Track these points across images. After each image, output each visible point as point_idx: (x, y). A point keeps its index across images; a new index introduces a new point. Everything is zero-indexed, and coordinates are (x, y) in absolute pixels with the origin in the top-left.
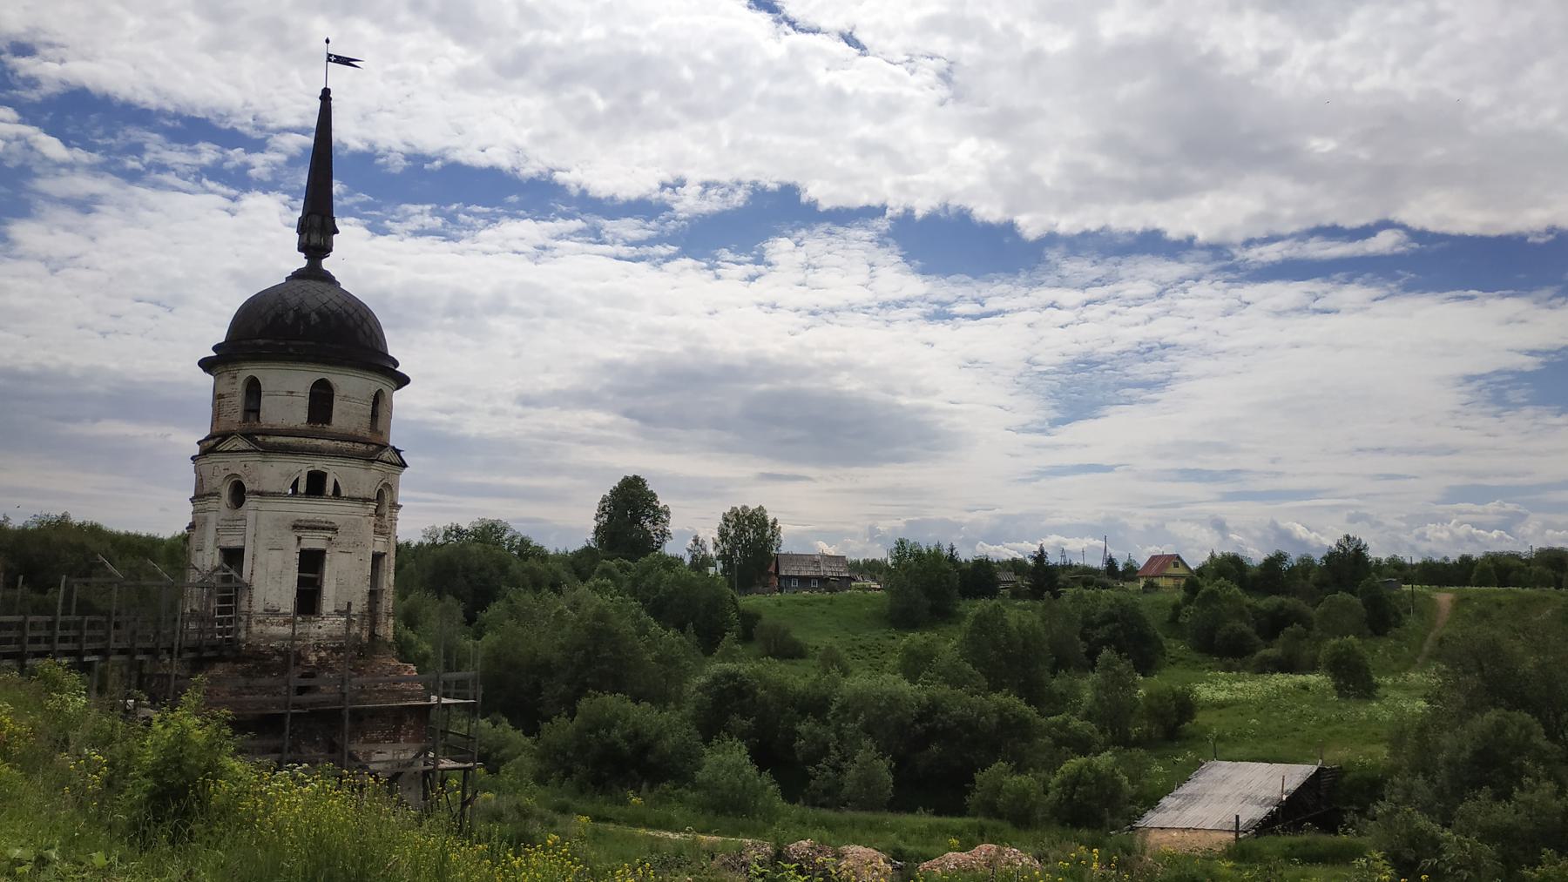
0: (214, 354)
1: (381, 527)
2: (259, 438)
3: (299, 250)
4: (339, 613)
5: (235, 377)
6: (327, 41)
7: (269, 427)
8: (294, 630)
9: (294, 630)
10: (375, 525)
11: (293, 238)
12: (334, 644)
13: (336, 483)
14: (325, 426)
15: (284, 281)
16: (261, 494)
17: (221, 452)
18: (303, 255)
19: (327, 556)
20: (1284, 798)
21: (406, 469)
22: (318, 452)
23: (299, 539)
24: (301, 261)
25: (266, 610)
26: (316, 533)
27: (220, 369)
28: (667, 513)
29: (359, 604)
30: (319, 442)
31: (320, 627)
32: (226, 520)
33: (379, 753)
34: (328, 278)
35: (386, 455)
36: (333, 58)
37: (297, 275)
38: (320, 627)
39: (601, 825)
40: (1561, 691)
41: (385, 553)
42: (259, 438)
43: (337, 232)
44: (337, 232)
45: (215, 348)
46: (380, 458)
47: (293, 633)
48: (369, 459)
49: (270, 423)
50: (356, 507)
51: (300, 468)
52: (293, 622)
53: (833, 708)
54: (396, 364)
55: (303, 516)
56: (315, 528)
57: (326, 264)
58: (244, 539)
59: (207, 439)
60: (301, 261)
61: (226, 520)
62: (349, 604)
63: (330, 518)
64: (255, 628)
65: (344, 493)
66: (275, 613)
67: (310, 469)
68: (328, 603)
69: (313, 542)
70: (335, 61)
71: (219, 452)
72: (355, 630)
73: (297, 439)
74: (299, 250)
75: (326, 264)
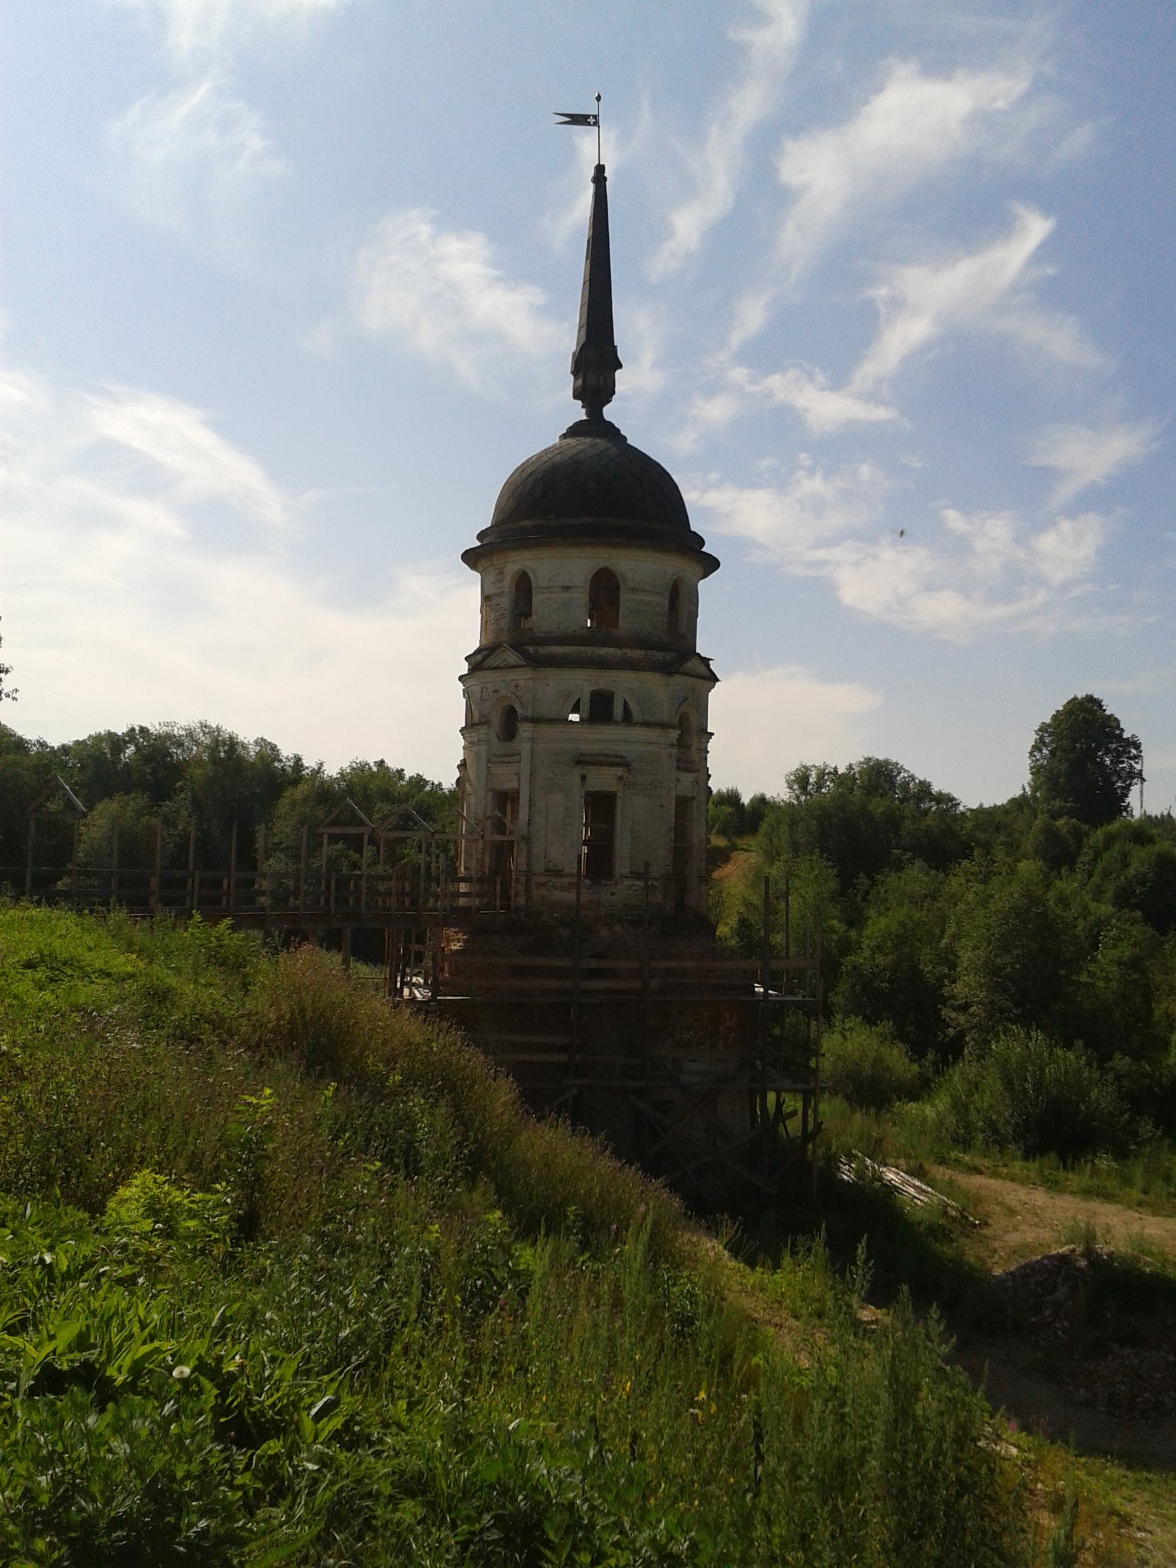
0: (479, 544)
1: (687, 762)
2: (531, 649)
3: (575, 397)
4: (635, 875)
5: (501, 573)
6: (599, 98)
7: (544, 635)
8: (578, 896)
9: (578, 896)
10: (678, 761)
11: (568, 383)
12: (632, 916)
13: (626, 706)
14: (610, 629)
15: (557, 440)
16: (535, 720)
17: (489, 669)
18: (580, 403)
19: (619, 802)
20: (713, 477)
21: (718, 684)
22: (603, 664)
23: (583, 778)
24: (579, 413)
25: (547, 870)
26: (606, 770)
27: (484, 563)
28: (1137, 746)
29: (661, 863)
30: (604, 651)
31: (613, 894)
32: (499, 756)
33: (691, 1061)
34: (612, 432)
35: (691, 664)
36: (592, 120)
37: (575, 430)
38: (613, 894)
39: (666, 1348)
40: (1088, 835)
41: (693, 798)
42: (531, 649)
43: (620, 366)
44: (620, 366)
45: (480, 536)
46: (681, 671)
47: (578, 900)
48: (667, 669)
49: (543, 629)
50: (653, 734)
51: (583, 682)
52: (577, 886)
53: (598, 1528)
54: (702, 542)
55: (586, 748)
56: (602, 764)
57: (610, 412)
58: (519, 779)
59: (476, 653)
60: (579, 413)
61: (499, 756)
62: (647, 864)
63: (621, 749)
64: (537, 893)
65: (636, 716)
66: (559, 873)
67: (594, 688)
68: (622, 867)
69: (604, 779)
70: (589, 116)
71: (486, 669)
72: (659, 898)
73: (575, 648)
74: (575, 397)
75: (610, 412)
